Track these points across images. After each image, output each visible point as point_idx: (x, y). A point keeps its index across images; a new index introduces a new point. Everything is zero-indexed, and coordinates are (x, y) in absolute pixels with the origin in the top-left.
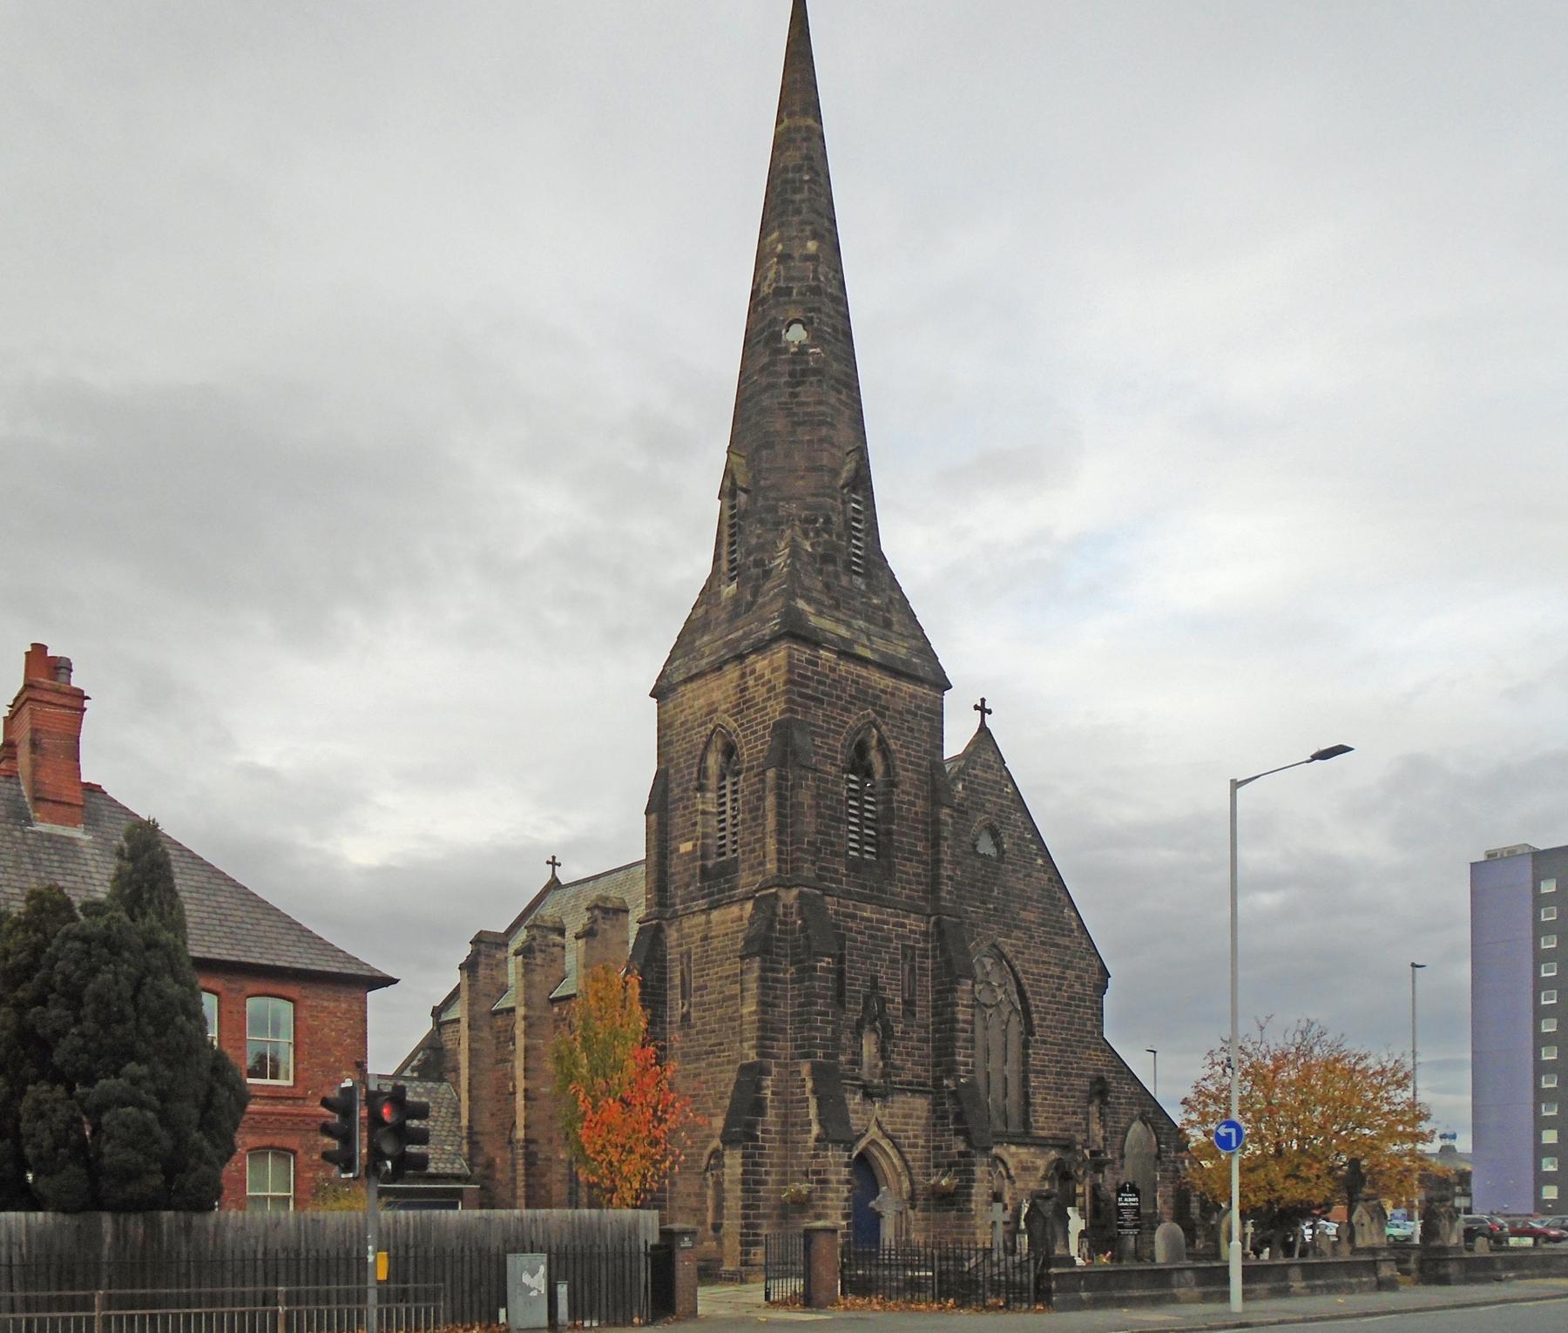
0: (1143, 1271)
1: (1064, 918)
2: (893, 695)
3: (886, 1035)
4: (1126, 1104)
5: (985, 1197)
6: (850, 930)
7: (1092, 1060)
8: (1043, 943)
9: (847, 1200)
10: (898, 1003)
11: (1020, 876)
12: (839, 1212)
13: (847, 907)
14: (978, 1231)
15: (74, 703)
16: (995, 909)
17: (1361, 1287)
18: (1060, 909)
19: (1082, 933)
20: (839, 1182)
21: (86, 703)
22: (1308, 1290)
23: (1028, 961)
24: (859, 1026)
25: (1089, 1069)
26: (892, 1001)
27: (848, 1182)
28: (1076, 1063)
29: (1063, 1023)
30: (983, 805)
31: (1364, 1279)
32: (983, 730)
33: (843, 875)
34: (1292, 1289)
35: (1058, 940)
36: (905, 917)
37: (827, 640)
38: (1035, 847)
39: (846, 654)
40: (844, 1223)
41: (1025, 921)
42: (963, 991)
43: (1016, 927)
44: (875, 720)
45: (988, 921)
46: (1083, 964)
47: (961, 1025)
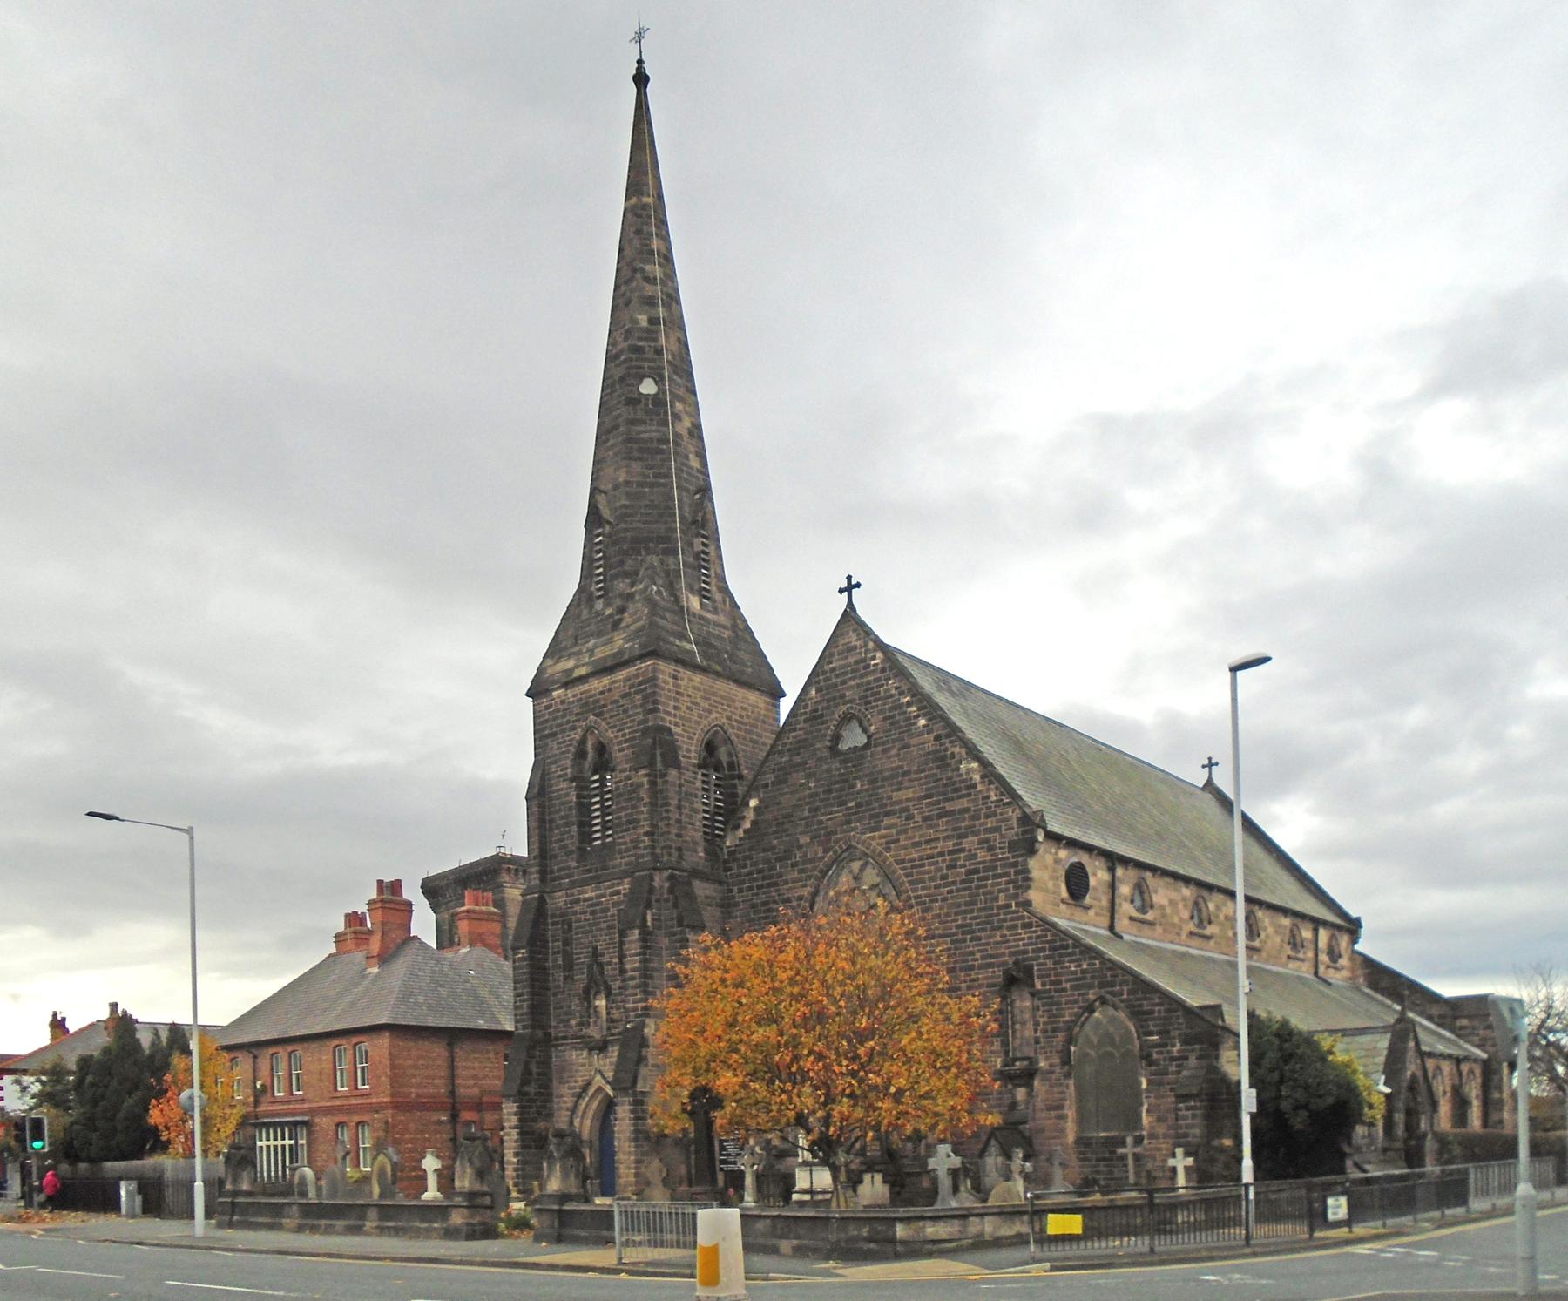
0: (788, 1217)
1: (962, 775)
2: (610, 690)
3: (608, 994)
4: (1074, 988)
5: (628, 1134)
6: (575, 913)
7: (1008, 941)
8: (925, 819)
9: (516, 1141)
10: (616, 964)
11: (894, 752)
12: (512, 1151)
13: (572, 895)
14: (621, 1166)
15: (408, 908)
16: (858, 805)
17: (427, 1234)
18: (954, 766)
19: (991, 783)
20: (511, 1128)
21: (414, 908)
22: (378, 1231)
23: (905, 848)
24: (587, 991)
25: (1003, 955)
26: (609, 963)
27: (516, 1127)
28: (980, 951)
29: (959, 906)
30: (843, 696)
31: (436, 1225)
32: (849, 615)
33: (575, 868)
34: (365, 1228)
35: (949, 806)
36: (619, 884)
37: (554, 682)
38: (915, 709)
39: (569, 683)
40: (515, 1160)
41: (900, 802)
42: (631, 942)
43: (887, 814)
44: (595, 722)
45: (849, 822)
46: (990, 823)
47: (630, 974)
